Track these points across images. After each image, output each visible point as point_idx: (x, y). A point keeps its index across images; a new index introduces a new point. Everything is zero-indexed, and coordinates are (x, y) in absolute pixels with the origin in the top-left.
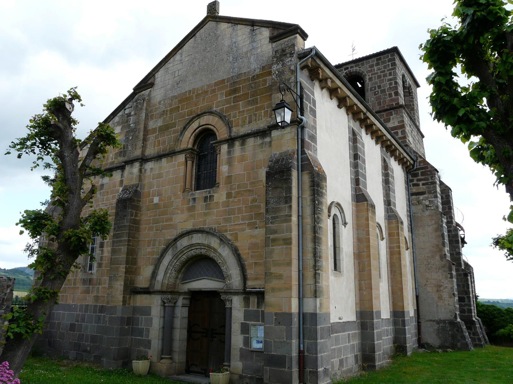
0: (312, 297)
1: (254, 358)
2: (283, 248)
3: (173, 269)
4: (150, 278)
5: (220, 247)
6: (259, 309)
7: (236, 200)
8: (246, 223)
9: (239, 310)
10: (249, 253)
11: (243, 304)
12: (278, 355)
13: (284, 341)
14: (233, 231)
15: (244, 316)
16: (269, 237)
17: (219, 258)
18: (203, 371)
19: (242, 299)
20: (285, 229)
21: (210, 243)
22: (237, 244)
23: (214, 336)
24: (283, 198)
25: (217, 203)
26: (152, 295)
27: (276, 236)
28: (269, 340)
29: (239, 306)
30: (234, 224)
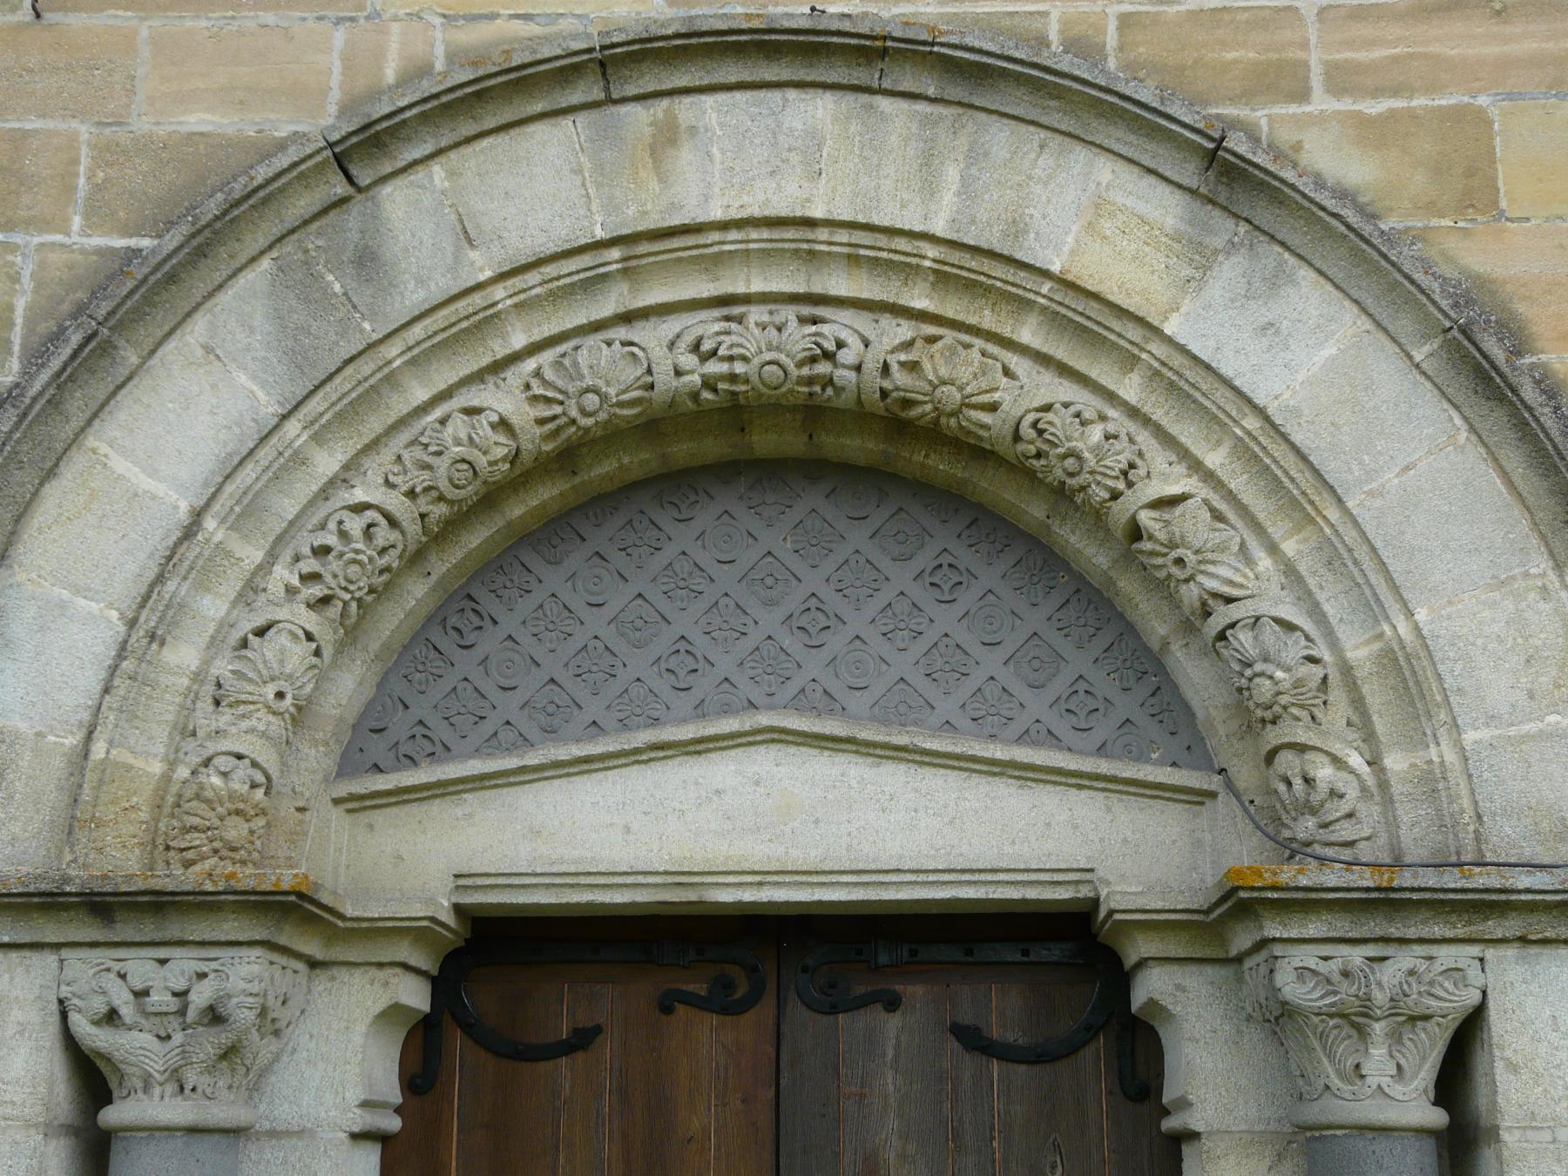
3: (283, 574)
5: (1194, 284)
14: (1395, 92)
17: (1144, 438)
21: (1017, 229)
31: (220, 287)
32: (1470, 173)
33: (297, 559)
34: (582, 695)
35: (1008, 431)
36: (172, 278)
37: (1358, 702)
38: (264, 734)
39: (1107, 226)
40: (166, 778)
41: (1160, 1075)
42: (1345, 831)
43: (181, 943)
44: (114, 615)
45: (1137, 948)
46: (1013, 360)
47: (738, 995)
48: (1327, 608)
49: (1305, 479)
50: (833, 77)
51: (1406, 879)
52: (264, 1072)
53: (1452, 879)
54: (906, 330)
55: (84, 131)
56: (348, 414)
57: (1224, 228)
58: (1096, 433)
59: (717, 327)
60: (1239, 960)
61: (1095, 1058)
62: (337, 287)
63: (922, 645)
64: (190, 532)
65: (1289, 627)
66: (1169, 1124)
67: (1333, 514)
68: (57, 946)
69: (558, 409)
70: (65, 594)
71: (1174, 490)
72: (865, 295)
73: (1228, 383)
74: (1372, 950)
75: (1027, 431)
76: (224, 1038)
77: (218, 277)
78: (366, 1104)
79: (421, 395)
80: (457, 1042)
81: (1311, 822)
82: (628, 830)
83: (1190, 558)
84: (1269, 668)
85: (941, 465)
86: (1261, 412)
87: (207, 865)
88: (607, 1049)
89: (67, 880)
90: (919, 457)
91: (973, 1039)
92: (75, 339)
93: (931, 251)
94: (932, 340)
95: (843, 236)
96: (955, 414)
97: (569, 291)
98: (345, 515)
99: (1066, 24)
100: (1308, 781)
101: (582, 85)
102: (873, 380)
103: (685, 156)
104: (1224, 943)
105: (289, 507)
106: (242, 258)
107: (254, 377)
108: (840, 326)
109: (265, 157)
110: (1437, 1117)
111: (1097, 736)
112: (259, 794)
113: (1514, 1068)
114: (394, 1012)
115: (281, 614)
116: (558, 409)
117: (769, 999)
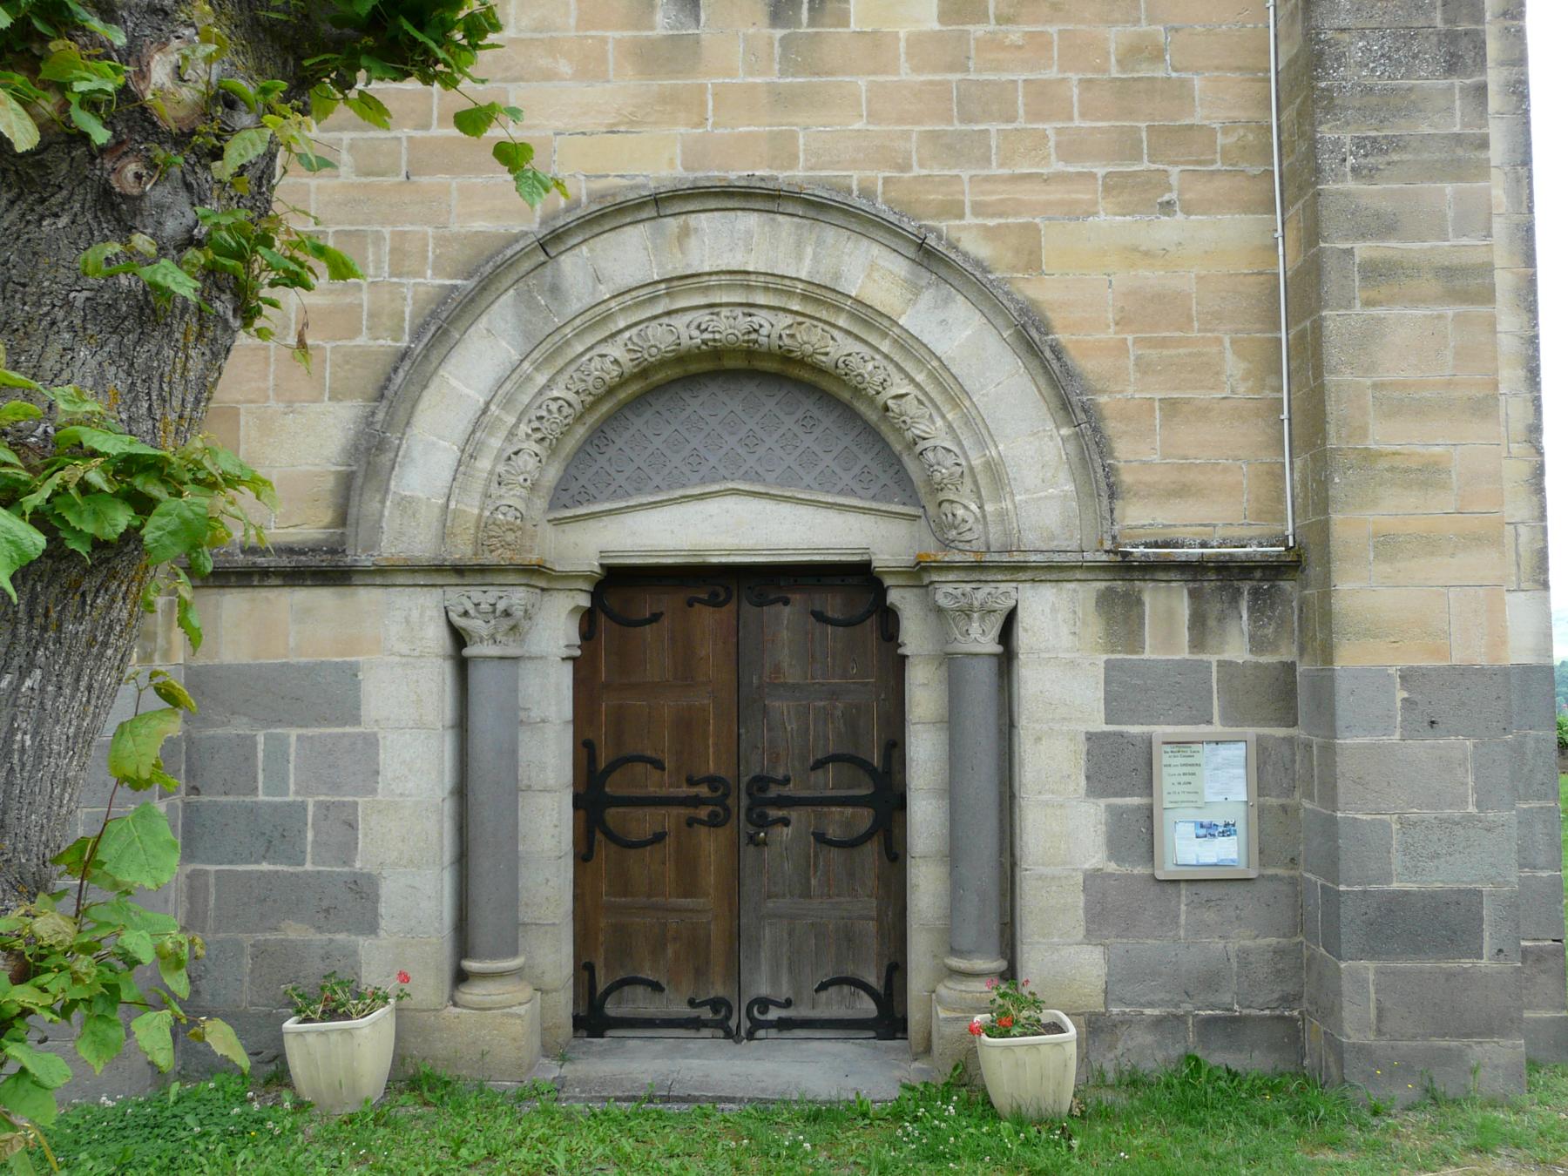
0: (1523, 586)
1: (1183, 918)
2: (1440, 317)
3: (524, 428)
4: (330, 483)
5: (912, 302)
6: (1204, 657)
7: (1015, 34)
8: (1093, 176)
9: (1073, 664)
10: (1122, 347)
11: (1095, 628)
12: (1433, 895)
13: (1470, 818)
14: (1001, 215)
15: (1109, 699)
16: (1350, 252)
17: (890, 368)
18: (706, 1013)
19: (1091, 603)
20: (1450, 214)
21: (837, 276)
22: (1033, 290)
23: (774, 813)
24: (1434, 39)
25: (876, 41)
26: (362, 592)
27: (1392, 248)
28: (1369, 817)
29: (1066, 640)
30: (1005, 171)
31: (492, 303)
32: (1031, 253)
33: (530, 421)
34: (652, 475)
35: (833, 364)
36: (472, 300)
37: (975, 482)
38: (520, 497)
39: (876, 275)
40: (480, 516)
41: (898, 630)
42: (968, 536)
43: (492, 585)
44: (455, 448)
45: (888, 582)
46: (836, 333)
47: (721, 598)
48: (964, 443)
49: (956, 388)
50: (757, 206)
51: (988, 558)
52: (527, 633)
53: (1005, 557)
54: (789, 320)
55: (430, 231)
56: (549, 358)
57: (926, 278)
58: (870, 366)
59: (708, 318)
60: (927, 586)
61: (871, 623)
62: (543, 302)
63: (799, 451)
64: (484, 412)
65: (949, 451)
66: (900, 651)
67: (967, 403)
68: (442, 586)
69: (639, 355)
70: (435, 439)
71: (903, 391)
72: (772, 304)
73: (925, 346)
74: (974, 585)
75: (841, 364)
76: (510, 622)
77: (491, 299)
78: (567, 646)
79: (580, 349)
80: (602, 619)
81: (954, 532)
82: (672, 532)
83: (909, 421)
84: (939, 468)
85: (806, 375)
86: (939, 359)
87: (500, 551)
88: (665, 622)
89: (445, 560)
90: (797, 371)
91: (820, 617)
92: (433, 329)
93: (800, 286)
94: (800, 324)
95: (762, 279)
96: (811, 356)
97: (644, 302)
98: (550, 402)
99: (860, 181)
100: (954, 515)
101: (647, 210)
102: (775, 342)
103: (693, 242)
104: (921, 580)
105: (526, 399)
106: (502, 290)
107: (509, 343)
108: (761, 318)
109: (509, 245)
110: (999, 649)
111: (872, 492)
112: (519, 521)
113: (1026, 630)
114: (577, 608)
115: (524, 446)
116: (639, 355)
117: (734, 599)
